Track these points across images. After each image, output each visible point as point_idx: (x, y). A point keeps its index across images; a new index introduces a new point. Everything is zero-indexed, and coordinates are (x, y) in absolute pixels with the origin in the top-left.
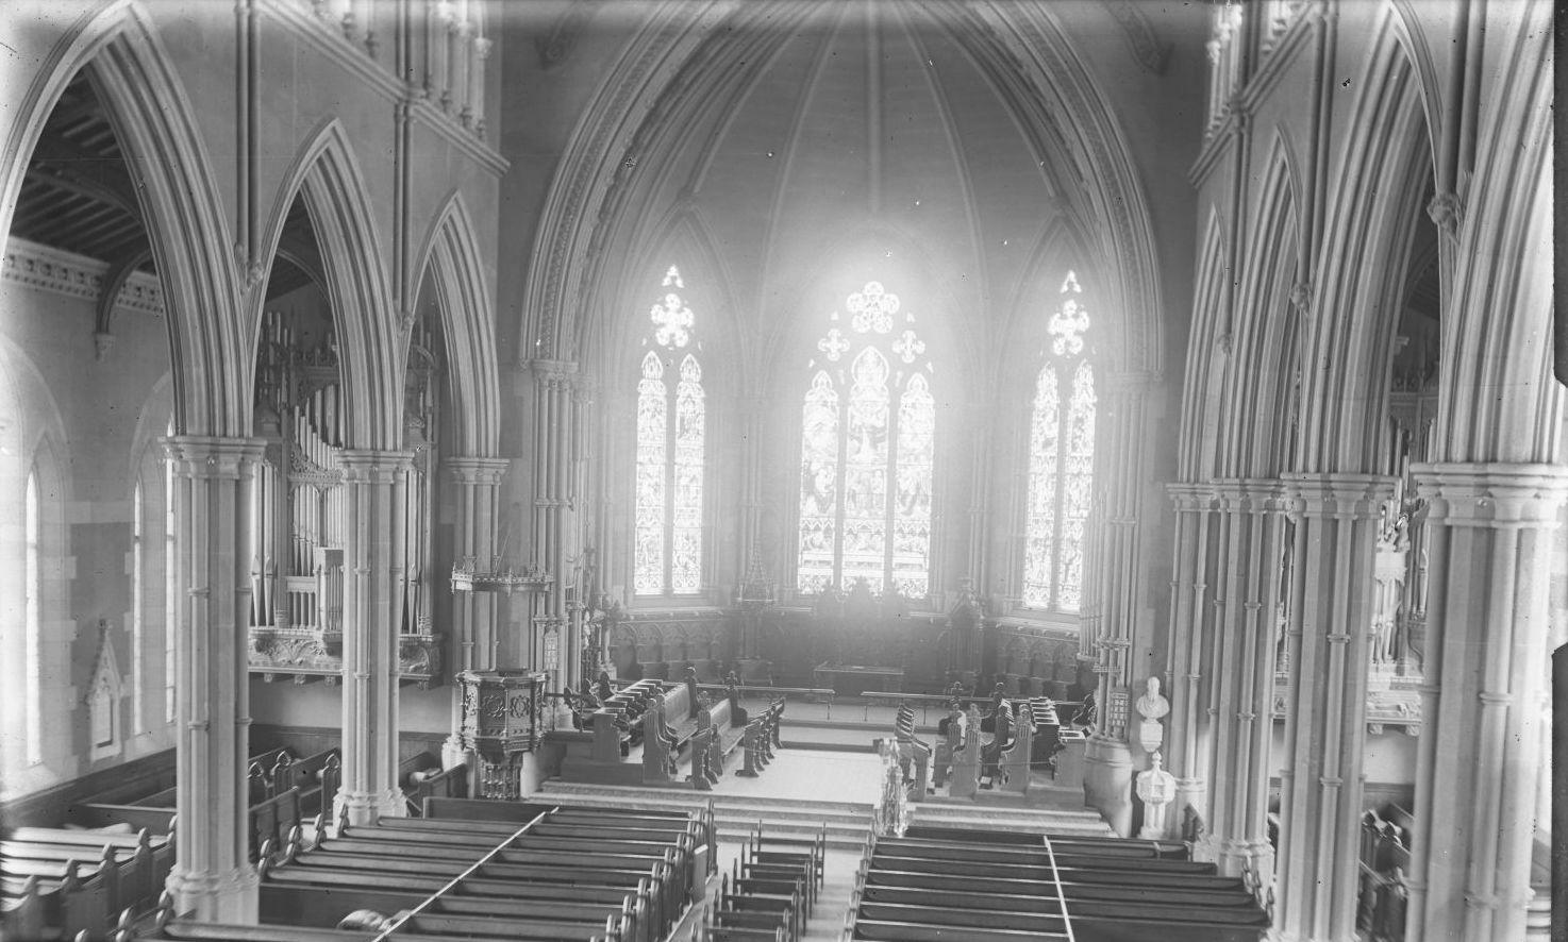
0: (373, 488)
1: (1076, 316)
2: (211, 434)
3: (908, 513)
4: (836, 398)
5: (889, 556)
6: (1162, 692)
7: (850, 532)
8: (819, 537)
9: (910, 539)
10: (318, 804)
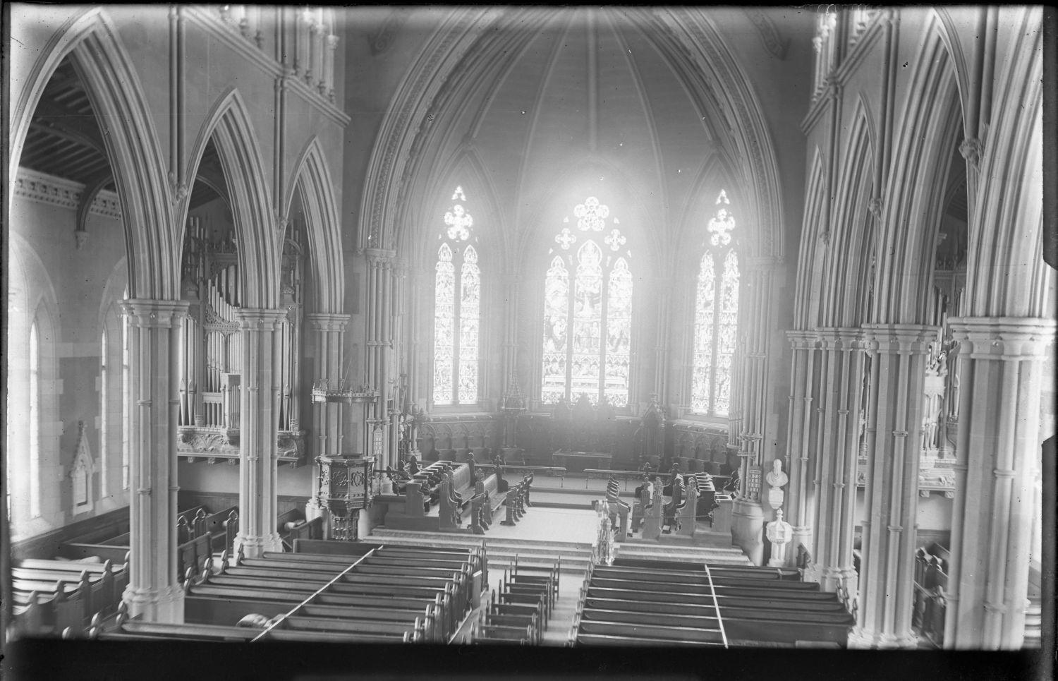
0: (260, 334)
1: (726, 220)
2: (153, 298)
3: (615, 350)
4: (567, 274)
5: (602, 379)
6: (783, 469)
7: (576, 363)
8: (556, 366)
9: (616, 368)
10: (223, 543)
